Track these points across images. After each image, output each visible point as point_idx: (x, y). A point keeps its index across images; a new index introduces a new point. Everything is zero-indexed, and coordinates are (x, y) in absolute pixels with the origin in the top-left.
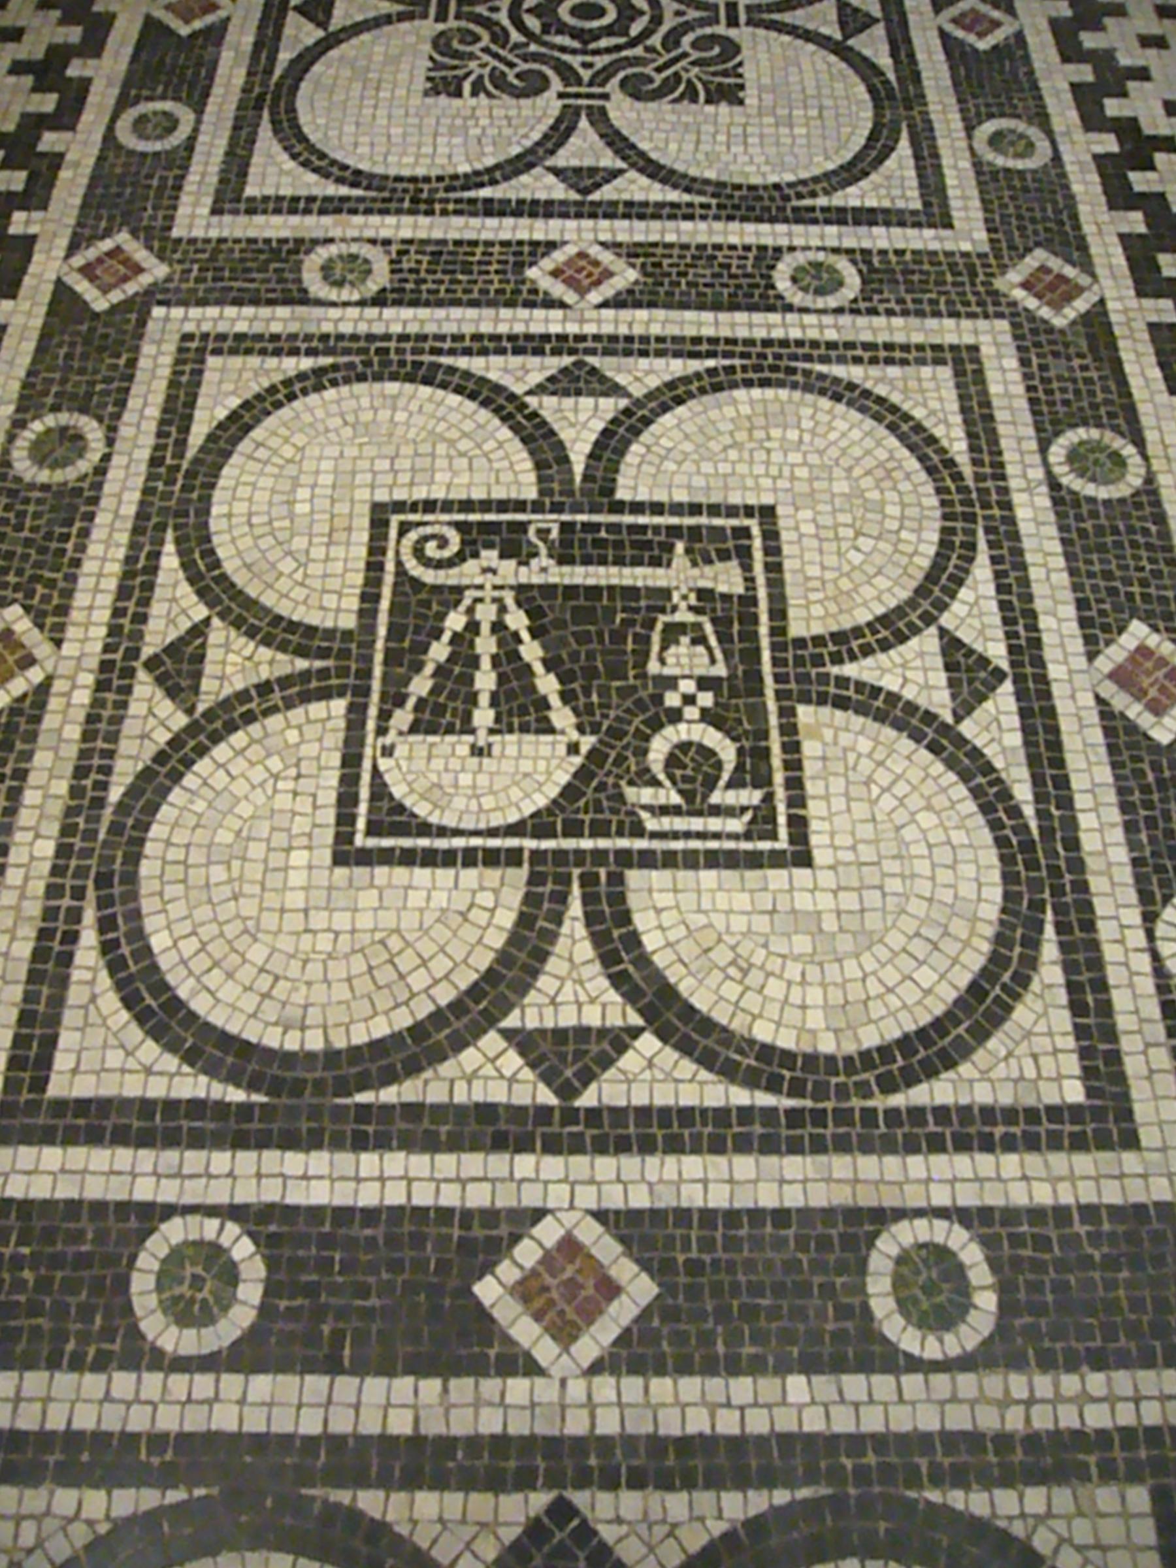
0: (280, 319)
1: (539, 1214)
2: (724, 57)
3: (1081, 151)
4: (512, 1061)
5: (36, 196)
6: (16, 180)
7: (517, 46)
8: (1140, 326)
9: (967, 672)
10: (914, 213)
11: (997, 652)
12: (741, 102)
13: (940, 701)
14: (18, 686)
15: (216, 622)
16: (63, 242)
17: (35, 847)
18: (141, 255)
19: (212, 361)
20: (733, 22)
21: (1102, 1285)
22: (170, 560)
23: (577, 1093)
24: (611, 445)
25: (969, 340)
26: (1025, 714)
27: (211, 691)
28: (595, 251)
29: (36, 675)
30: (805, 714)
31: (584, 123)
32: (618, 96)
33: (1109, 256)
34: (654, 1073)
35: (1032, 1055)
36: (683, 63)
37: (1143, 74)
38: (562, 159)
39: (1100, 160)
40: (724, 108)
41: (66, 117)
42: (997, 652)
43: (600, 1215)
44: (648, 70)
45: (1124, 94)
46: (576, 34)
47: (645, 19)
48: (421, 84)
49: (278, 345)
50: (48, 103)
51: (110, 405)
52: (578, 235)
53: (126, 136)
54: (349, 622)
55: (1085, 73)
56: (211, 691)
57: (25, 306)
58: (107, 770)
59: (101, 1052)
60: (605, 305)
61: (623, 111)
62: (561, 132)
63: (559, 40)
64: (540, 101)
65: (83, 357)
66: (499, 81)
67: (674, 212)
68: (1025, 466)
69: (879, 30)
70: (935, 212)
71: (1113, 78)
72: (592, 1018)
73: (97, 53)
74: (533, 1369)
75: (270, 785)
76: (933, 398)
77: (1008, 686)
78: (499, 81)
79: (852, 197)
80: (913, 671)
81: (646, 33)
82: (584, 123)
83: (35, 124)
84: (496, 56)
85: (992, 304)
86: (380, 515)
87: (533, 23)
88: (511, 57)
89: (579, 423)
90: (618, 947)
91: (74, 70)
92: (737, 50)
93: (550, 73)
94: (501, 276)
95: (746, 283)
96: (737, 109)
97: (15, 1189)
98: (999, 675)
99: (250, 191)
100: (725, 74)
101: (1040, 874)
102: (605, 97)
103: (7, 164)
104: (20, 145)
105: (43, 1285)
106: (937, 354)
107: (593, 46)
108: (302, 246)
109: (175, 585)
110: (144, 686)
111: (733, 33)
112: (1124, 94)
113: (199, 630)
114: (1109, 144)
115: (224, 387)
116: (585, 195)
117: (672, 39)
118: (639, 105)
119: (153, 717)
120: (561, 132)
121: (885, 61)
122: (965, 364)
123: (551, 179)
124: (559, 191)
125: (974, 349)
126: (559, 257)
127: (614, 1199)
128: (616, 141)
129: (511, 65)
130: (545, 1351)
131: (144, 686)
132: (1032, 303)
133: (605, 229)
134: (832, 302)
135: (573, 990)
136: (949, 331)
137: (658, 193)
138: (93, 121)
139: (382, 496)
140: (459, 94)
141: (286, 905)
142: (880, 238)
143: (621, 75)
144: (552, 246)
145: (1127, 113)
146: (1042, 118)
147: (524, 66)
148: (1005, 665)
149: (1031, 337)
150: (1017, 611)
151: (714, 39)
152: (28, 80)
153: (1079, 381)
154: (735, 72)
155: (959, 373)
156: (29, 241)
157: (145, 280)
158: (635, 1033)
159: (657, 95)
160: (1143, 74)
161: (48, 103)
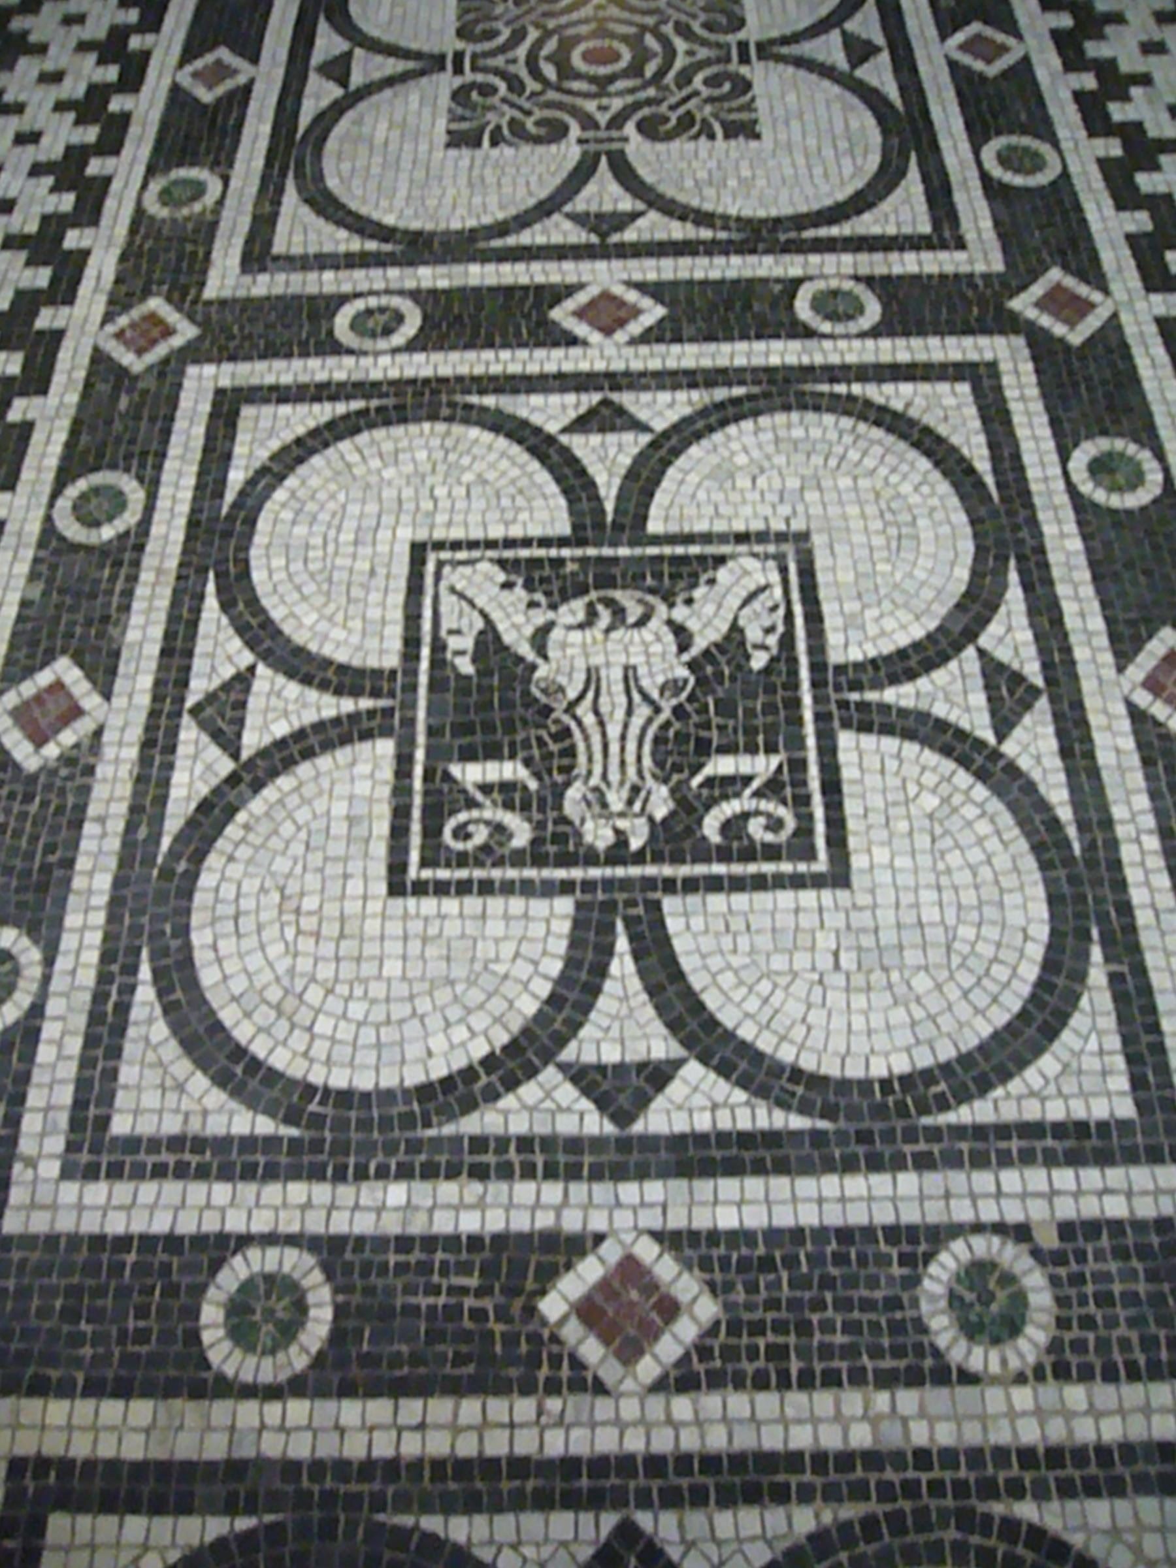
0: (317, 369)
3: (1082, 156)
4: (567, 1093)
7: (533, 94)
8: (1066, 95)
9: (1006, 692)
11: (1033, 671)
12: (757, 136)
13: (842, 63)
15: (261, 669)
18: (172, 316)
20: (744, 59)
24: (643, 479)
27: (252, 741)
33: (1115, 258)
34: (697, 1101)
35: (1080, 1071)
36: (673, 100)
37: (1145, 80)
39: (1103, 163)
42: (1033, 671)
44: (663, 108)
45: (1157, 167)
46: (612, 35)
47: (544, 52)
48: (441, 137)
50: (42, 277)
51: (149, 464)
52: (603, 276)
53: (153, 207)
54: (392, 661)
55: (1141, 221)
56: (252, 741)
62: (582, 174)
63: (576, 85)
66: (518, 131)
68: (1071, 569)
69: (885, 57)
70: (945, 230)
71: (1116, 82)
73: (43, 389)
76: (952, 411)
79: (867, 224)
80: (953, 693)
81: (661, 73)
82: (604, 160)
83: (28, 302)
84: (513, 105)
85: (1010, 324)
86: (418, 551)
87: (550, 71)
88: (527, 105)
89: (607, 459)
91: (116, 104)
92: (747, 86)
93: (567, 118)
94: (523, 316)
96: (754, 144)
100: (740, 109)
101: (1085, 895)
104: (13, 327)
109: (150, 1021)
110: (189, 733)
111: (744, 70)
112: (1157, 167)
113: (244, 679)
116: (604, 237)
117: (685, 78)
118: (661, 147)
119: (197, 767)
120: (582, 174)
121: (892, 91)
122: (983, 380)
123: (568, 225)
124: (577, 235)
125: (993, 366)
126: (582, 298)
131: (189, 733)
135: (623, 1024)
137: (678, 231)
139: (422, 535)
141: (349, 949)
144: (570, 290)
148: (1039, 682)
149: (1043, 349)
151: (728, 76)
153: (1093, 389)
154: (749, 107)
155: (977, 391)
156: (26, 428)
157: (177, 341)
159: (669, 137)
160: (1145, 80)
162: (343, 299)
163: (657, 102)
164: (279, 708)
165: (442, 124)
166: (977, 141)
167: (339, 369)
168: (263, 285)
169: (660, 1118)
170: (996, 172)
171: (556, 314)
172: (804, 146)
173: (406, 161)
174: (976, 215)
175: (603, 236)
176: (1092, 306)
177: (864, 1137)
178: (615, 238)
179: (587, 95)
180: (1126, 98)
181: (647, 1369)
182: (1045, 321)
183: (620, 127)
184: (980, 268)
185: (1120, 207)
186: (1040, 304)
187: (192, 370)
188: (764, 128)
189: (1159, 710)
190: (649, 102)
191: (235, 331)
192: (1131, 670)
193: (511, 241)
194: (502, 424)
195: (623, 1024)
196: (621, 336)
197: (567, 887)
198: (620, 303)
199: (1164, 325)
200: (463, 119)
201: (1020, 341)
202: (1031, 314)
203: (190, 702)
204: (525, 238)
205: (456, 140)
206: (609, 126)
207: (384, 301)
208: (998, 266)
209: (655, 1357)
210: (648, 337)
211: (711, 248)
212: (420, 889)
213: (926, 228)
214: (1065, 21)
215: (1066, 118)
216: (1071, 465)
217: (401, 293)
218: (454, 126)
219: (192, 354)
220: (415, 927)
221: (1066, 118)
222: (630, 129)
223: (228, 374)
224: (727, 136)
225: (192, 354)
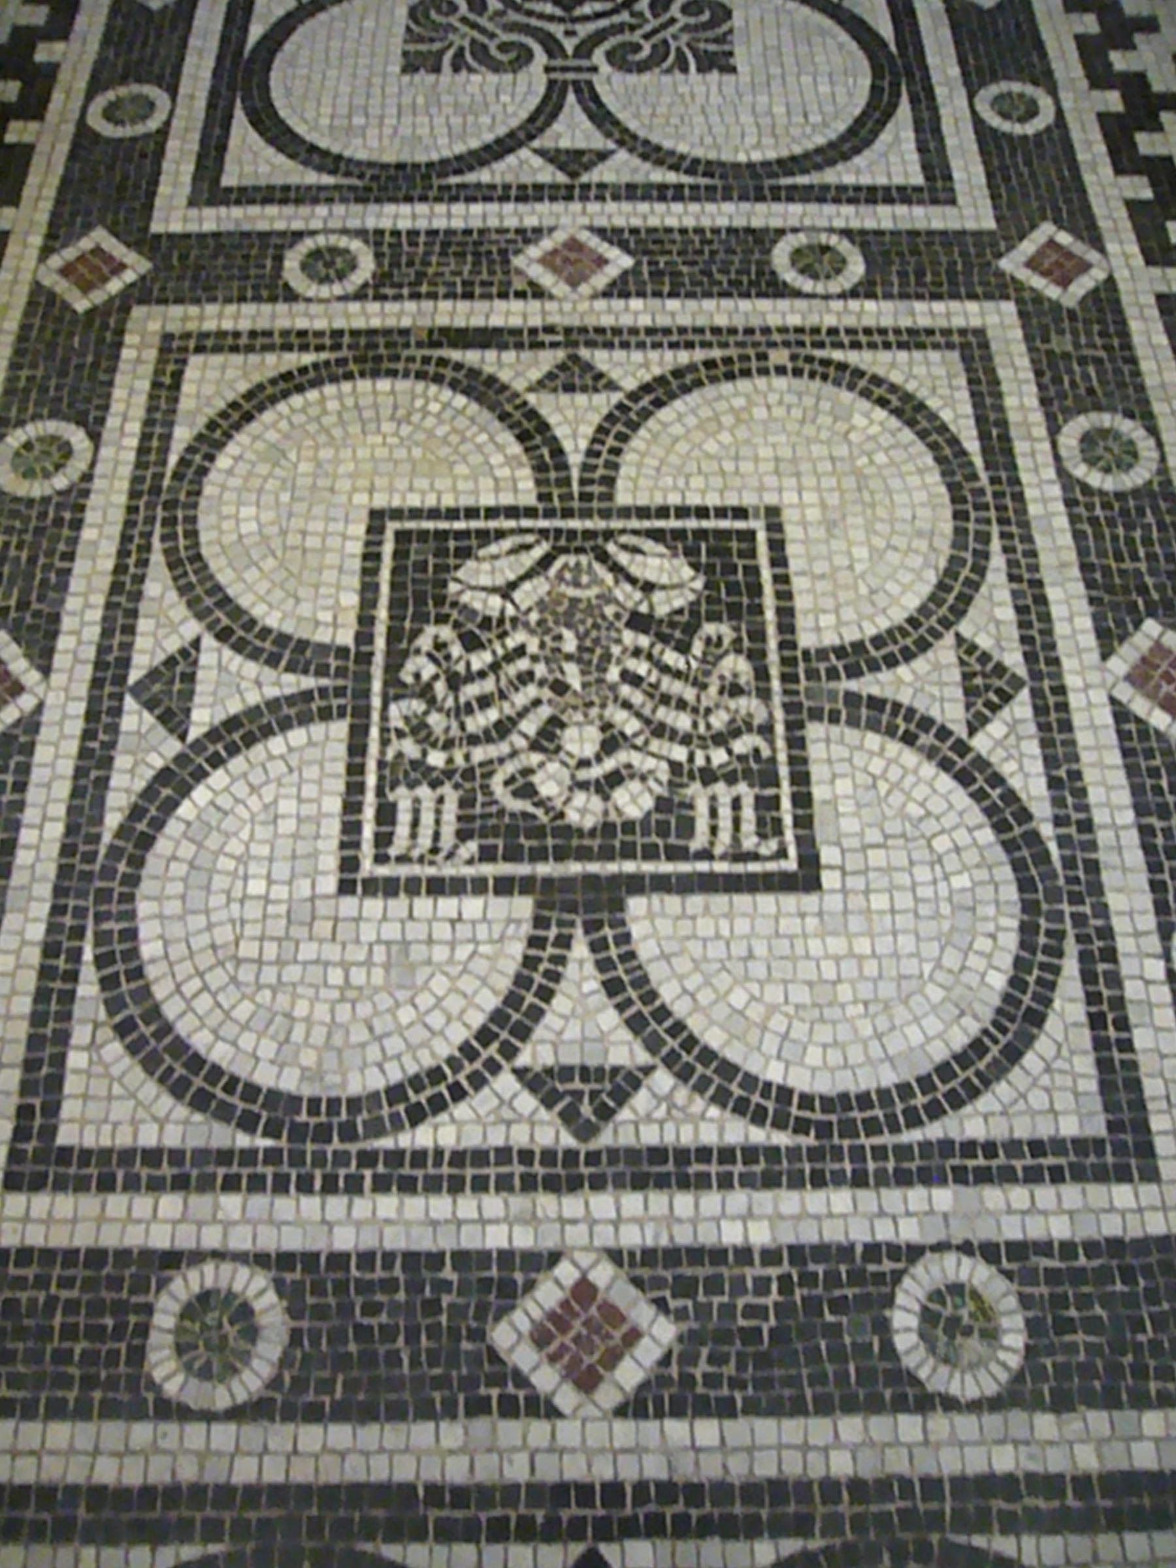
1: (554, 1258)
2: (712, 24)
3: (1083, 108)
5: (33, 105)
6: (10, 90)
9: (986, 688)
10: (918, 189)
11: (1014, 660)
12: (733, 70)
13: (952, 712)
14: (10, 714)
16: (37, 240)
17: (31, 920)
19: (195, 360)
21: (1125, 1321)
25: (976, 322)
28: (584, 236)
31: (571, 97)
32: (605, 68)
35: (1051, 1093)
36: (648, 28)
39: (1103, 118)
40: (714, 76)
42: (1014, 660)
43: (615, 1256)
44: (636, 37)
49: (259, 341)
52: (570, 220)
53: (96, 121)
55: (1113, 101)
56: (202, 719)
58: (113, 1006)
66: (481, 52)
67: (677, 194)
70: (937, 185)
75: (271, 816)
77: (1024, 694)
78: (481, 52)
80: (929, 684)
82: (571, 97)
84: (474, 26)
85: (1001, 288)
88: (490, 26)
90: (626, 983)
91: (42, 54)
94: (483, 263)
95: (741, 265)
96: (729, 79)
98: (1017, 683)
99: (228, 180)
101: (1053, 887)
105: (59, 1330)
107: (578, 12)
110: (135, 718)
113: (190, 652)
114: (1113, 101)
115: (209, 384)
118: (632, 79)
119: (143, 747)
122: (974, 350)
123: (537, 161)
124: (548, 174)
125: (980, 332)
126: (547, 244)
127: (631, 1237)
128: (601, 117)
129: (492, 36)
132: (1038, 282)
133: (621, 214)
134: (834, 287)
136: (966, 313)
138: (64, 102)
141: (297, 933)
142: (884, 217)
144: (538, 232)
145: (1136, 67)
146: (1046, 79)
147: (506, 37)
148: (1022, 671)
149: (1037, 318)
150: (1032, 608)
153: (1087, 360)
155: (967, 360)
157: (129, 276)
162: (298, 235)
163: (633, 28)
164: (229, 684)
165: (397, 45)
168: (210, 220)
172: (784, 85)
173: (352, 86)
174: (968, 169)
175: (574, 175)
177: (849, 1129)
179: (551, 18)
180: (1130, 46)
182: (1038, 282)
183: (589, 55)
184: (971, 225)
185: (1119, 170)
186: (1032, 264)
187: (138, 312)
188: (739, 60)
189: (1140, 706)
190: (620, 29)
191: (192, 268)
193: (470, 178)
197: (526, 885)
199: (1164, 301)
200: (421, 39)
202: (1024, 275)
204: (484, 176)
205: (411, 66)
206: (577, 53)
208: (990, 224)
211: (696, 194)
212: (372, 887)
213: (918, 179)
214: (1090, 24)
215: (1066, 64)
216: (1062, 440)
218: (411, 47)
219: (142, 293)
221: (1066, 64)
222: (598, 56)
223: (179, 317)
224: (700, 70)
225: (141, 293)
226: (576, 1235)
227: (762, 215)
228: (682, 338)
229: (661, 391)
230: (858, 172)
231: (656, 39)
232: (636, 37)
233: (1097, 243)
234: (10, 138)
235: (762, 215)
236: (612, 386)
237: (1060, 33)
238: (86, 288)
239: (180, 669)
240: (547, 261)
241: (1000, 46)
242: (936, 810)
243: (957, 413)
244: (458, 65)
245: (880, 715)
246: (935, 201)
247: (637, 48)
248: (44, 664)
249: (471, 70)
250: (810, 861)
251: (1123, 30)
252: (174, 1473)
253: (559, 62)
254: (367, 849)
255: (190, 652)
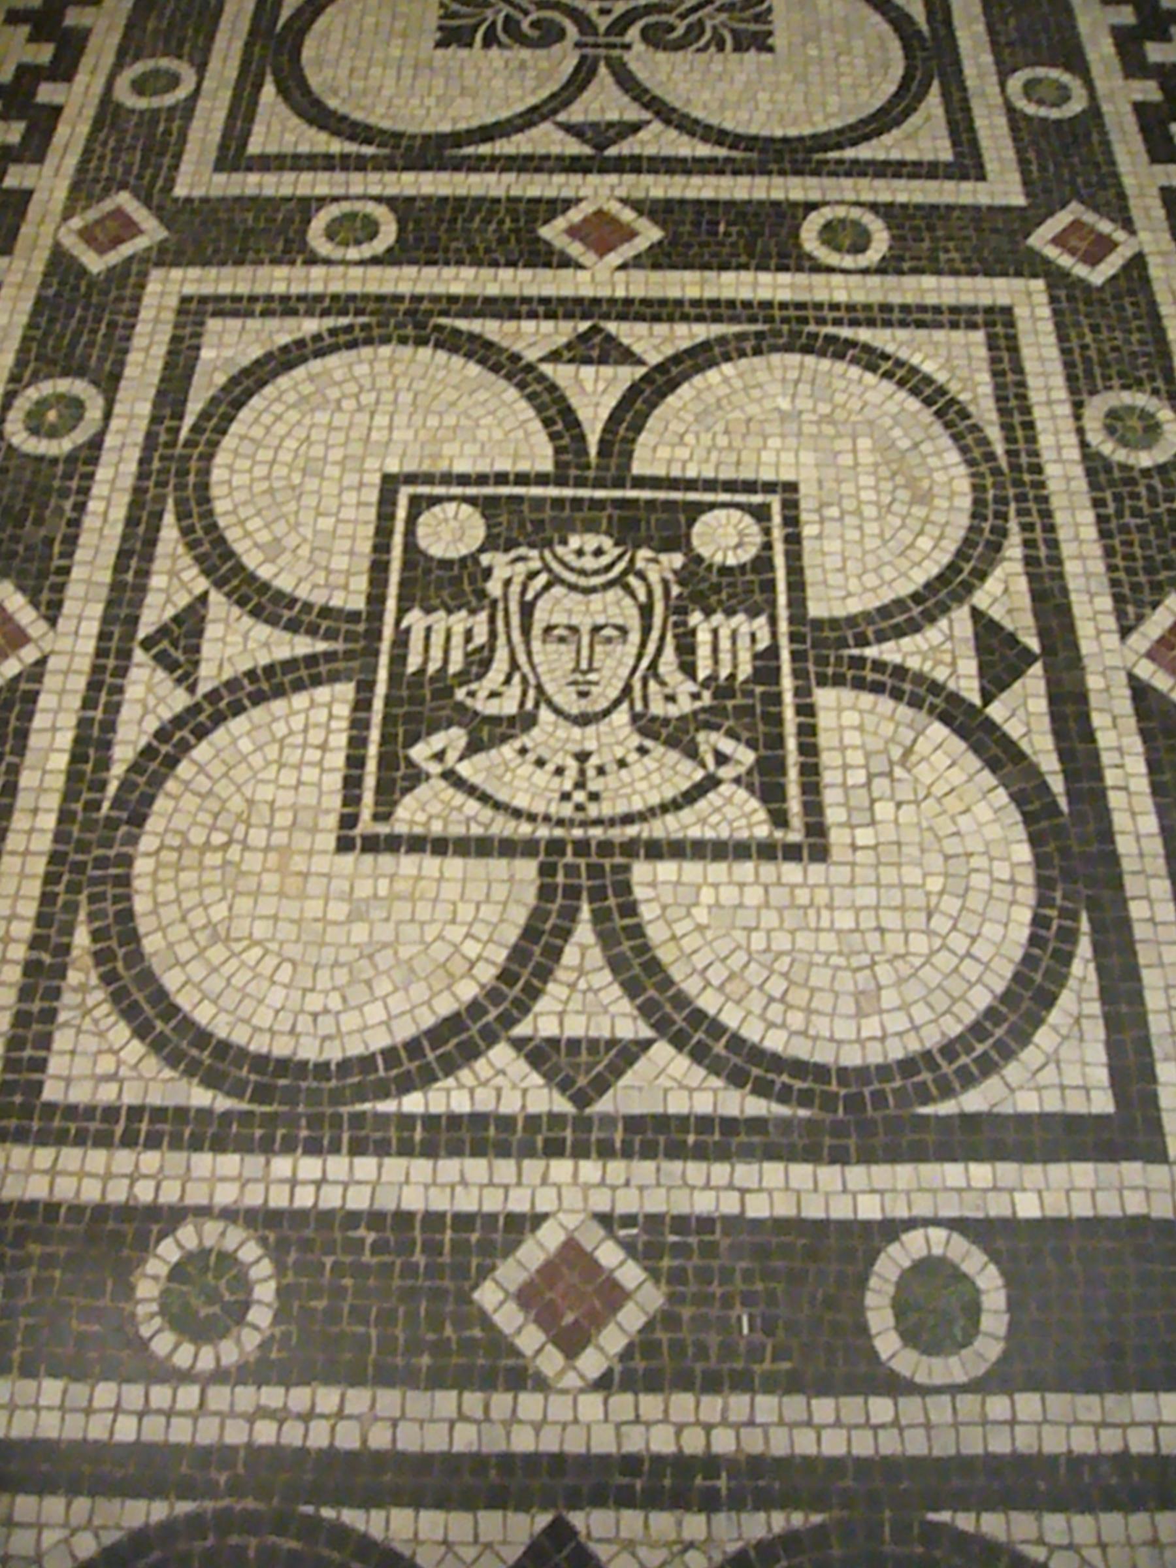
0: (279, 280)
5: (35, 147)
9: (999, 657)
10: (948, 165)
12: (770, 49)
14: (12, 667)
22: (169, 531)
23: (589, 1102)
25: (1003, 300)
26: (1054, 699)
27: (209, 676)
29: (29, 654)
30: (824, 697)
31: (603, 70)
32: (639, 47)
34: (669, 1082)
35: (1063, 1067)
38: (575, 114)
39: (1140, 108)
40: (751, 56)
41: (63, 69)
44: (670, 18)
50: (44, 54)
52: (599, 192)
53: (124, 95)
57: (18, 263)
59: (94, 1057)
60: (623, 267)
61: (645, 62)
64: (557, 49)
65: (77, 325)
70: (968, 163)
72: (602, 1030)
73: (68, 77)
74: (542, 1384)
77: (1037, 669)
80: (942, 651)
82: (603, 70)
83: (29, 75)
86: (390, 484)
89: (594, 393)
94: (516, 235)
95: (766, 236)
97: (12, 1191)
102: (627, 47)
103: (5, 117)
104: (16, 96)
106: (958, 317)
108: (307, 206)
113: (198, 607)
115: (227, 347)
116: (600, 150)
118: (661, 56)
119: (149, 698)
122: (998, 325)
123: (560, 135)
125: (1008, 311)
126: (575, 215)
128: (626, 81)
130: (551, 1362)
139: (393, 467)
140: (470, 45)
141: (302, 913)
143: (640, 24)
146: (1076, 62)
149: (1067, 295)
152: (25, 30)
153: (1109, 332)
157: (139, 244)
158: (646, 1045)
159: (678, 46)
161: (44, 54)
164: (235, 643)
166: (1004, 73)
167: (316, 281)
169: (630, 1095)
170: (1022, 104)
171: (545, 232)
172: (817, 67)
173: (386, 62)
175: (600, 147)
176: (1114, 245)
178: (612, 151)
181: (592, 1363)
182: (1065, 260)
183: (622, 32)
186: (1057, 241)
191: (206, 234)
192: (1133, 639)
194: (482, 352)
195: (583, 1000)
196: (614, 258)
198: (614, 221)
201: (1038, 285)
202: (1051, 252)
203: (141, 634)
206: (608, 32)
207: (358, 206)
208: (1020, 200)
209: (601, 1349)
210: (556, 207)
213: (947, 155)
215: (1101, 51)
216: (1087, 412)
217: (378, 199)
219: (164, 256)
220: (779, 896)
221: (1101, 51)
222: (633, 34)
226: (65, 644)
227: (795, 189)
228: (713, 310)
229: (700, 358)
230: (888, 149)
231: (693, 18)
232: (670, 18)
233: (1128, 225)
234: (10, 182)
235: (795, 189)
236: (640, 362)
237: (1096, 30)
238: (102, 251)
239: (188, 626)
240: (573, 232)
241: (1032, 24)
242: (690, 899)
243: (978, 393)
244: (490, 40)
245: (898, 684)
246: (965, 177)
247: (672, 28)
248: (52, 613)
249: (501, 45)
250: (817, 829)
251: (1156, 23)
252: (364, 1441)
253: (590, 39)
254: (366, 812)
255: (198, 607)
